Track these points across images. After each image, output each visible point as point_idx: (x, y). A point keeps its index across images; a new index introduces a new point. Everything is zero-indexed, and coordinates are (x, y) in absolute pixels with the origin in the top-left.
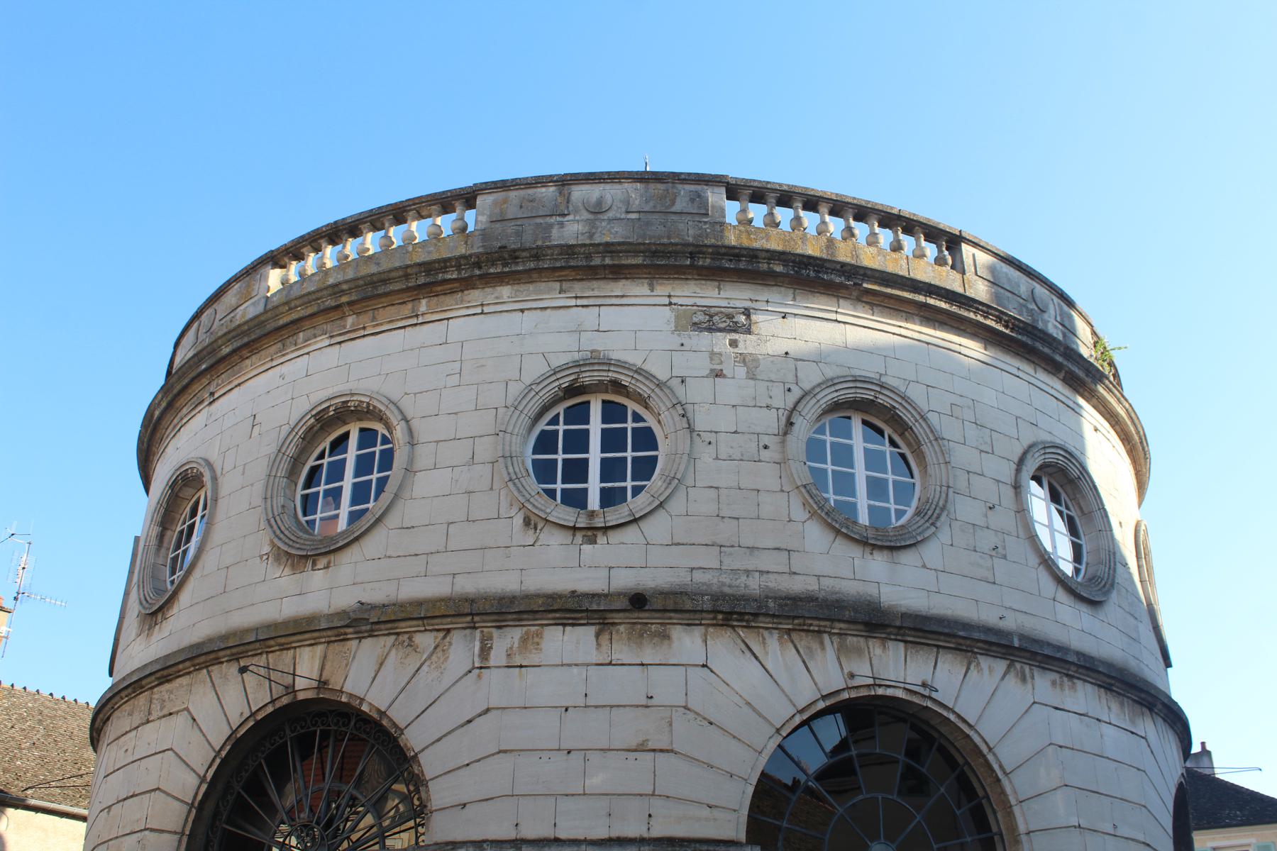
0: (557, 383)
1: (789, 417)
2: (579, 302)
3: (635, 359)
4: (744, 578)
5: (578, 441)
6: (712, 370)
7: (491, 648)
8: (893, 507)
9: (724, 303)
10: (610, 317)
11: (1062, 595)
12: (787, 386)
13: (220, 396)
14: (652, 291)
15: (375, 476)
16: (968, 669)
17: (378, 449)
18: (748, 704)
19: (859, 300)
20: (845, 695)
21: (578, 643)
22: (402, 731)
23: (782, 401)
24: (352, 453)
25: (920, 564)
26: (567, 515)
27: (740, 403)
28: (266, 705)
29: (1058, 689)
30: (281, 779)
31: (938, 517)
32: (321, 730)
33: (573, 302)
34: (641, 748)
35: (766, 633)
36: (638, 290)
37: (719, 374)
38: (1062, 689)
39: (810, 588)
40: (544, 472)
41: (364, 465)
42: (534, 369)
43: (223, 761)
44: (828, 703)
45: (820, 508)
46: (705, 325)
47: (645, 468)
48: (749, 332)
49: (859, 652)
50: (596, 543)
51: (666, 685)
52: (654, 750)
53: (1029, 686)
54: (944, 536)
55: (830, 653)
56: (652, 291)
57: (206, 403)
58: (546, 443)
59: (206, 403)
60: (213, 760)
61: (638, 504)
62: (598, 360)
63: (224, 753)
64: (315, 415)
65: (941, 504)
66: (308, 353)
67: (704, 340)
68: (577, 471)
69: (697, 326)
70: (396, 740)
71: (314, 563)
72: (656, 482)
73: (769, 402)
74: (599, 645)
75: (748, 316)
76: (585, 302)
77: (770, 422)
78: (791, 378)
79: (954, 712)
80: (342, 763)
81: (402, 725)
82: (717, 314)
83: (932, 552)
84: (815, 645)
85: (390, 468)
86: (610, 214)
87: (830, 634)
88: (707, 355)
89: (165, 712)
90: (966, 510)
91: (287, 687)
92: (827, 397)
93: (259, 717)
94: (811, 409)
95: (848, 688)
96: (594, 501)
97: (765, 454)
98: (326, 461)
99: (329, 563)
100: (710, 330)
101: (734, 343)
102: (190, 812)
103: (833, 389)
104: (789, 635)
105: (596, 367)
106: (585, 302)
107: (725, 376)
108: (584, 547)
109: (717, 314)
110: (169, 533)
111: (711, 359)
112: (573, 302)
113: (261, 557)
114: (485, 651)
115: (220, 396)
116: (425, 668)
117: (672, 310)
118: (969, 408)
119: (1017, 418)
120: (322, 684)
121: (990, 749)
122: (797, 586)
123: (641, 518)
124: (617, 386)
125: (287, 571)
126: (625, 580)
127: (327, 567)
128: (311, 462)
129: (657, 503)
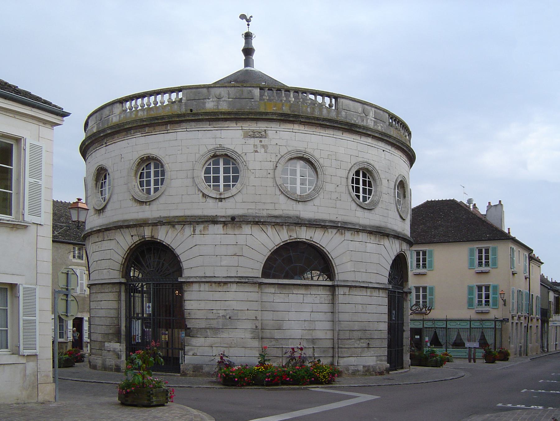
0: (210, 155)
1: (276, 164)
2: (215, 129)
3: (232, 147)
4: (262, 211)
5: (217, 171)
6: (254, 150)
7: (196, 229)
8: (307, 187)
9: (258, 129)
10: (224, 133)
11: (359, 209)
12: (276, 154)
13: (108, 145)
14: (237, 125)
16: (325, 232)
18: (262, 244)
19: (300, 124)
20: (289, 241)
21: (218, 229)
22: (174, 250)
23: (274, 159)
25: (313, 205)
26: (214, 194)
27: (263, 160)
28: (138, 241)
29: (353, 235)
31: (319, 191)
33: (213, 129)
34: (235, 255)
35: (267, 226)
36: (233, 124)
37: (256, 152)
38: (354, 235)
39: (280, 213)
42: (203, 150)
43: (128, 254)
44: (284, 243)
45: (284, 191)
46: (252, 136)
47: (236, 179)
48: (265, 138)
49: (293, 230)
50: (222, 202)
51: (241, 239)
52: (238, 256)
53: (344, 235)
54: (321, 196)
55: (285, 231)
56: (237, 125)
57: (104, 146)
58: (207, 171)
59: (104, 146)
60: (125, 254)
61: (233, 190)
62: (221, 147)
63: (128, 252)
64: (140, 159)
65: (321, 187)
66: (135, 138)
67: (252, 141)
68: (216, 179)
69: (251, 137)
70: (173, 252)
71: (146, 203)
72: (238, 184)
73: (271, 160)
74: (223, 229)
75: (265, 132)
76: (217, 129)
77: (271, 166)
78: (278, 152)
79: (319, 244)
81: (174, 248)
82: (256, 132)
83: (317, 202)
84: (281, 229)
86: (223, 99)
87: (285, 225)
88: (253, 146)
89: (109, 239)
90: (329, 187)
91: (143, 237)
92: (289, 157)
93: (136, 244)
94: (283, 161)
95: (289, 239)
96: (222, 188)
97: (269, 176)
99: (150, 203)
100: (254, 137)
101: (261, 141)
102: (121, 266)
103: (290, 155)
104: (274, 226)
105: (221, 150)
106: (217, 129)
107: (258, 152)
108: (219, 203)
109: (256, 132)
110: (98, 183)
111: (254, 147)
112: (213, 129)
113: (130, 199)
114: (194, 231)
115: (108, 145)
116: (179, 234)
117: (243, 131)
118: (334, 155)
119: (351, 155)
120: (152, 237)
121: (329, 253)
122: (276, 213)
123: (234, 195)
124: (226, 155)
125: (138, 205)
126: (230, 212)
127: (149, 205)
128: (141, 171)
129: (238, 191)
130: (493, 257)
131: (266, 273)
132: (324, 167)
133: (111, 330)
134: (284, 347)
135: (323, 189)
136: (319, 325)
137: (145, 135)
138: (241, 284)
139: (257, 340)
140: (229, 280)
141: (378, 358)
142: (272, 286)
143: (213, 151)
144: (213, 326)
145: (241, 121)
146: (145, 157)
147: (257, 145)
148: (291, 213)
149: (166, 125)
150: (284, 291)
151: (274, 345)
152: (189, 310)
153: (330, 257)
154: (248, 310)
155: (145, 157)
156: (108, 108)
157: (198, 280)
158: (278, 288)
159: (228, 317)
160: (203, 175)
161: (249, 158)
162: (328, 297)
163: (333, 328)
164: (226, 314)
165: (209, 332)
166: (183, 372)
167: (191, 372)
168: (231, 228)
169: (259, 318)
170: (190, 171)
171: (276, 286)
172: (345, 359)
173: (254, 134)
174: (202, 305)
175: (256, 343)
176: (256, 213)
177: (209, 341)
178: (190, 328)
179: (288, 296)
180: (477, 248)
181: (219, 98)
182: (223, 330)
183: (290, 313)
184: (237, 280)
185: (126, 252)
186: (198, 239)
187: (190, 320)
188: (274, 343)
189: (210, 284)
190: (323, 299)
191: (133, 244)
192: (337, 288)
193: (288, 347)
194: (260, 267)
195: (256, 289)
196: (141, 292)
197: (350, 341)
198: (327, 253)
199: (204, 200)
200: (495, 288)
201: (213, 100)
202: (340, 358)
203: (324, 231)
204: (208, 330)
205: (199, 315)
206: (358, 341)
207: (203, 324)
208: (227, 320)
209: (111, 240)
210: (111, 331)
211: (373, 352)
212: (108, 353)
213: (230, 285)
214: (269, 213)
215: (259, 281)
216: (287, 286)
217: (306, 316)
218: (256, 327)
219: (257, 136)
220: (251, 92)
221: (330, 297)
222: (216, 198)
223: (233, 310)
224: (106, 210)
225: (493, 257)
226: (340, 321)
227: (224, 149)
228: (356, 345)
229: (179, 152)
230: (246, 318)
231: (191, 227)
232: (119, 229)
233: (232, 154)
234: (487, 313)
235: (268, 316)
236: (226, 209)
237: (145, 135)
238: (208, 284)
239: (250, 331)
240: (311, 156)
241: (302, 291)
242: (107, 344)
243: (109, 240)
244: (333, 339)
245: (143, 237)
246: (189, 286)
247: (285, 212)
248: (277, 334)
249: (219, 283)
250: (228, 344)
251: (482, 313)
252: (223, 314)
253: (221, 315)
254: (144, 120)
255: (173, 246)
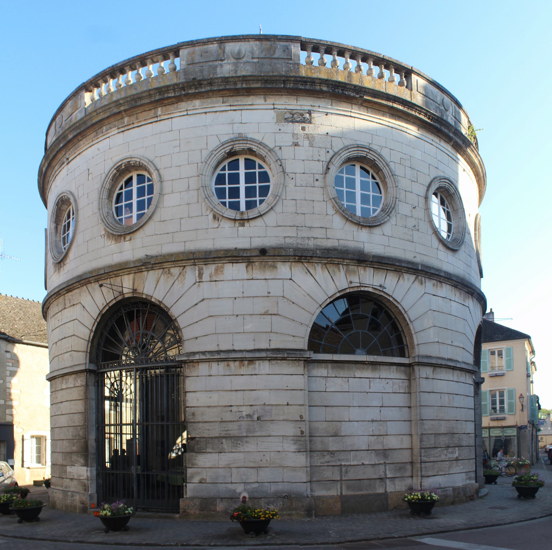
0: (224, 150)
1: (328, 165)
2: (232, 108)
3: (258, 137)
4: (307, 241)
5: (235, 179)
9: (299, 108)
10: (247, 115)
11: (441, 247)
12: (327, 150)
14: (265, 101)
15: (146, 197)
16: (399, 279)
17: (146, 184)
19: (362, 105)
20: (348, 291)
22: (169, 309)
23: (325, 157)
24: (135, 187)
25: (382, 234)
26: (231, 214)
28: (112, 300)
30: (123, 330)
32: (136, 310)
34: (266, 314)
35: (316, 265)
36: (258, 101)
37: (296, 145)
39: (335, 245)
40: (220, 193)
41: (141, 192)
42: (214, 143)
47: (264, 191)
49: (354, 272)
51: (275, 288)
53: (424, 286)
54: (393, 221)
56: (265, 101)
57: (66, 164)
58: (220, 180)
61: (261, 208)
63: (98, 320)
64: (116, 169)
65: (392, 206)
66: (109, 137)
68: (235, 193)
70: (167, 313)
71: (125, 238)
72: (269, 198)
73: (319, 158)
74: (247, 271)
75: (310, 114)
77: (319, 168)
79: (392, 297)
80: (146, 322)
81: (169, 307)
82: (295, 114)
83: (387, 228)
85: (152, 193)
86: (245, 60)
87: (343, 265)
88: (291, 135)
89: (72, 304)
91: (120, 293)
92: (345, 155)
94: (338, 161)
95: (349, 288)
96: (243, 207)
97: (317, 183)
98: (124, 190)
99: (131, 238)
100: (292, 122)
101: (303, 129)
103: (348, 151)
104: (325, 265)
105: (241, 142)
107: (299, 146)
109: (295, 114)
110: (59, 226)
111: (293, 137)
112: (229, 108)
113: (101, 236)
114: (200, 275)
116: (176, 283)
117: (275, 112)
118: (408, 160)
119: (417, 182)
122: (329, 244)
126: (258, 243)
128: (117, 192)
129: (270, 207)
130: (508, 358)
131: (313, 346)
132: (397, 177)
133: (74, 446)
134: (343, 463)
135: (396, 210)
136: (392, 428)
137: (122, 129)
138: (275, 361)
139: (303, 455)
140: (257, 355)
141: (467, 475)
142: (324, 365)
143: (230, 144)
144: (232, 433)
145: (273, 95)
146: (123, 165)
147: (297, 134)
148: (352, 245)
149: (154, 108)
150: (342, 373)
151: (328, 462)
152: (193, 409)
153: (407, 319)
154: (288, 405)
155: (123, 165)
156: (70, 103)
157: (208, 356)
158: (333, 368)
159: (255, 417)
160: (214, 186)
161: (287, 154)
162: (403, 382)
163: (411, 431)
164: (252, 412)
165: (226, 444)
166: (183, 512)
167: (198, 512)
168: (260, 268)
169: (306, 417)
170: (193, 178)
171: (330, 365)
172: (431, 480)
173: (292, 117)
174: (215, 399)
175: (302, 460)
176: (298, 244)
177: (225, 459)
178: (195, 438)
179: (348, 381)
180: (489, 350)
181: (238, 57)
182: (247, 439)
183: (351, 408)
184: (270, 355)
185: (96, 320)
186: (206, 289)
187: (195, 425)
188: (328, 458)
189: (226, 363)
190: (396, 386)
191: (105, 306)
192: (416, 368)
193: (349, 463)
194: (305, 332)
195: (299, 368)
196: (133, 402)
197: (436, 451)
198: (403, 312)
199: (216, 224)
200: (511, 392)
201: (229, 62)
202: (424, 478)
203: (398, 277)
204: (224, 440)
205: (210, 415)
206: (445, 451)
207: (215, 431)
208: (255, 423)
209: (74, 305)
210: (75, 449)
211: (462, 467)
212: (71, 483)
213: (259, 365)
214: (318, 244)
215: (305, 356)
216: (346, 365)
217: (373, 414)
218: (302, 432)
219: (298, 119)
220: (288, 49)
221: (406, 383)
222: (235, 220)
223: (264, 404)
224: (68, 261)
225: (508, 358)
226: (423, 420)
227: (246, 139)
228: (443, 457)
229: (177, 150)
230: (285, 418)
231: (195, 270)
232: (85, 285)
233: (260, 148)
234: (504, 419)
235: (320, 414)
236: (251, 237)
237: (122, 129)
238: (223, 363)
239: (291, 440)
240: (377, 156)
241: (368, 373)
242: (69, 469)
243: (71, 306)
244: (411, 449)
245: (120, 293)
246: (193, 368)
247: (341, 242)
248: (333, 445)
249: (242, 360)
250: (255, 462)
251: (497, 419)
252: (247, 413)
253: (244, 414)
254: (121, 104)
255: (167, 302)
